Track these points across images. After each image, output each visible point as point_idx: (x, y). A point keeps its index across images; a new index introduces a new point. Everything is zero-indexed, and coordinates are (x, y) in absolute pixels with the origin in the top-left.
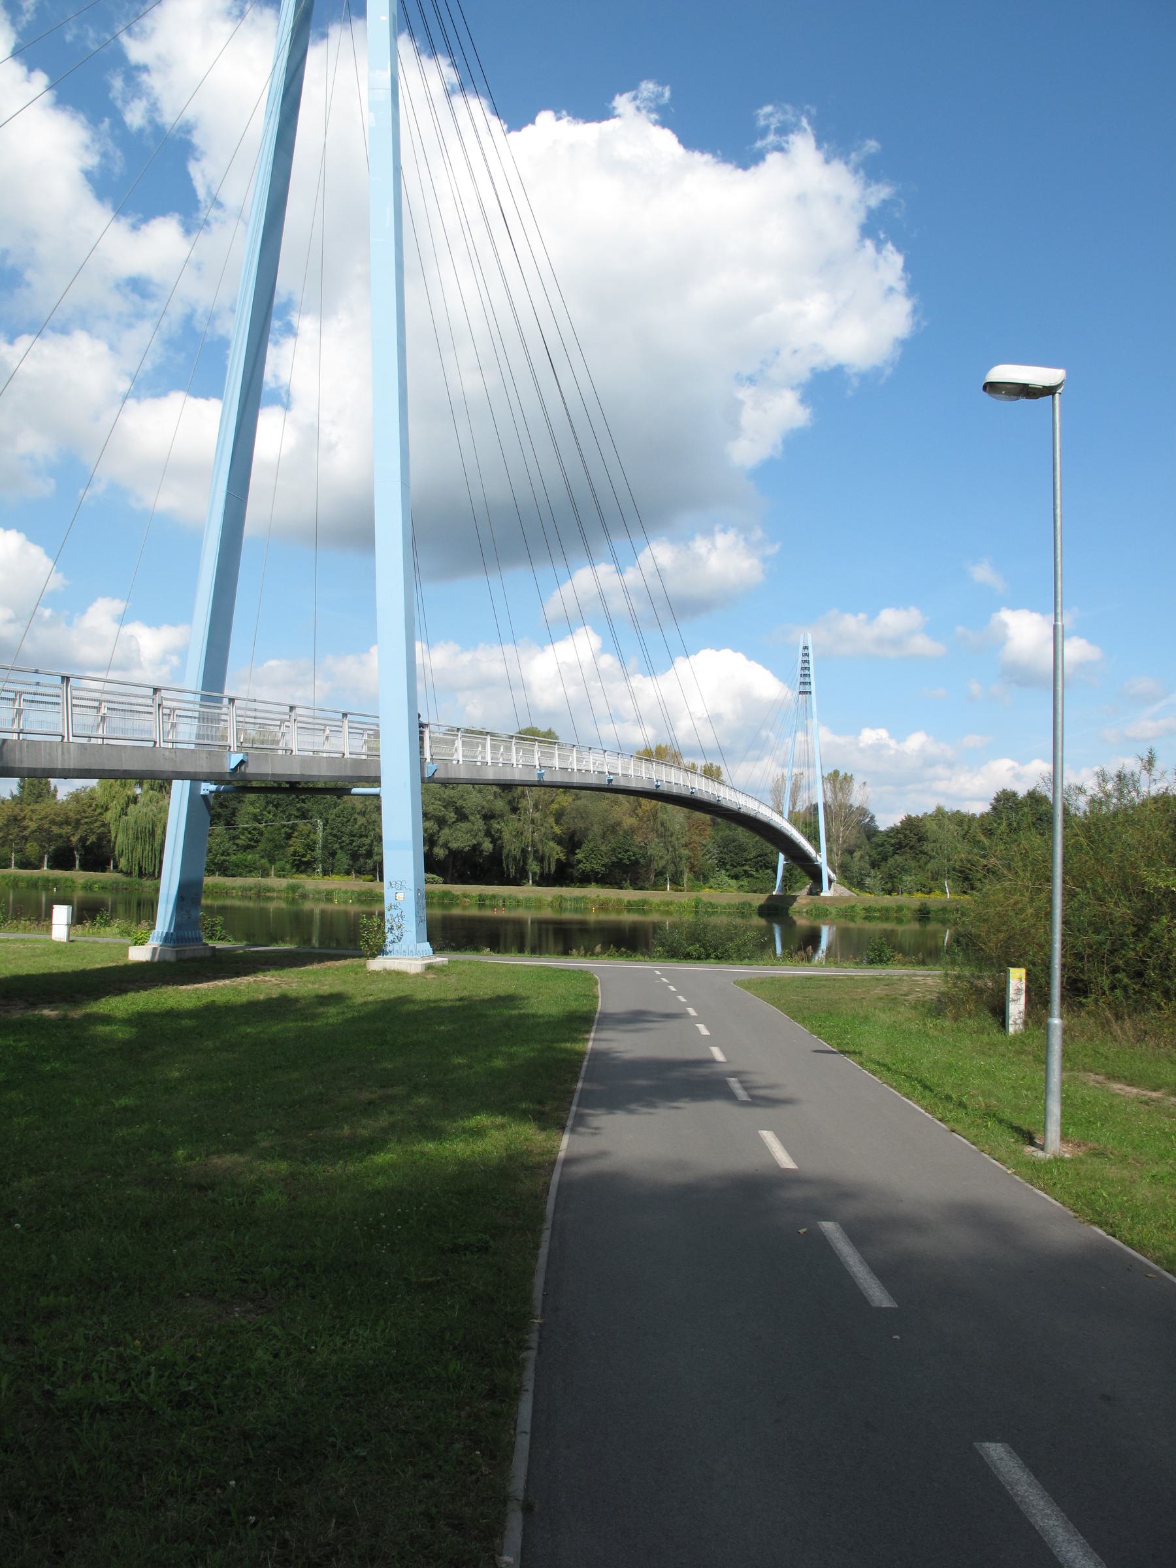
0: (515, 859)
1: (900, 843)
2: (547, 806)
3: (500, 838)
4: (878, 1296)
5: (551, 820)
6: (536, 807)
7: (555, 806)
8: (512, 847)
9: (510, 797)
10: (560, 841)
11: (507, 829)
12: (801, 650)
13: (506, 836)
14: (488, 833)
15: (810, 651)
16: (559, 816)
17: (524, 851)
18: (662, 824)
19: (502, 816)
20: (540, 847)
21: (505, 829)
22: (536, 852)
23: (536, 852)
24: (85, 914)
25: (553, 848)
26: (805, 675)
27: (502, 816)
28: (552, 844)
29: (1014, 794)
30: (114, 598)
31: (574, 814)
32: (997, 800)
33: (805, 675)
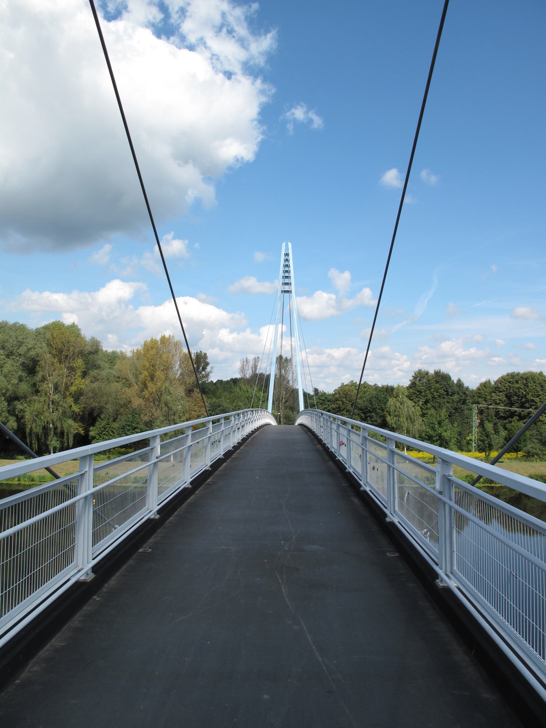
0: (37, 436)
1: (339, 408)
2: (67, 388)
3: (23, 417)
4: (474, 651)
5: (70, 400)
6: (56, 388)
7: (73, 389)
8: (33, 426)
9: (33, 382)
10: (75, 417)
11: (28, 410)
12: (283, 257)
13: (28, 416)
14: (12, 412)
15: (291, 257)
16: (77, 396)
17: (45, 429)
18: (166, 405)
19: (25, 397)
20: (59, 425)
21: (28, 410)
22: (56, 428)
23: (56, 428)
24: (475, 446)
25: (70, 426)
26: (287, 277)
27: (25, 397)
28: (70, 422)
29: (427, 373)
30: (60, 292)
31: (90, 394)
32: (415, 378)
33: (287, 277)
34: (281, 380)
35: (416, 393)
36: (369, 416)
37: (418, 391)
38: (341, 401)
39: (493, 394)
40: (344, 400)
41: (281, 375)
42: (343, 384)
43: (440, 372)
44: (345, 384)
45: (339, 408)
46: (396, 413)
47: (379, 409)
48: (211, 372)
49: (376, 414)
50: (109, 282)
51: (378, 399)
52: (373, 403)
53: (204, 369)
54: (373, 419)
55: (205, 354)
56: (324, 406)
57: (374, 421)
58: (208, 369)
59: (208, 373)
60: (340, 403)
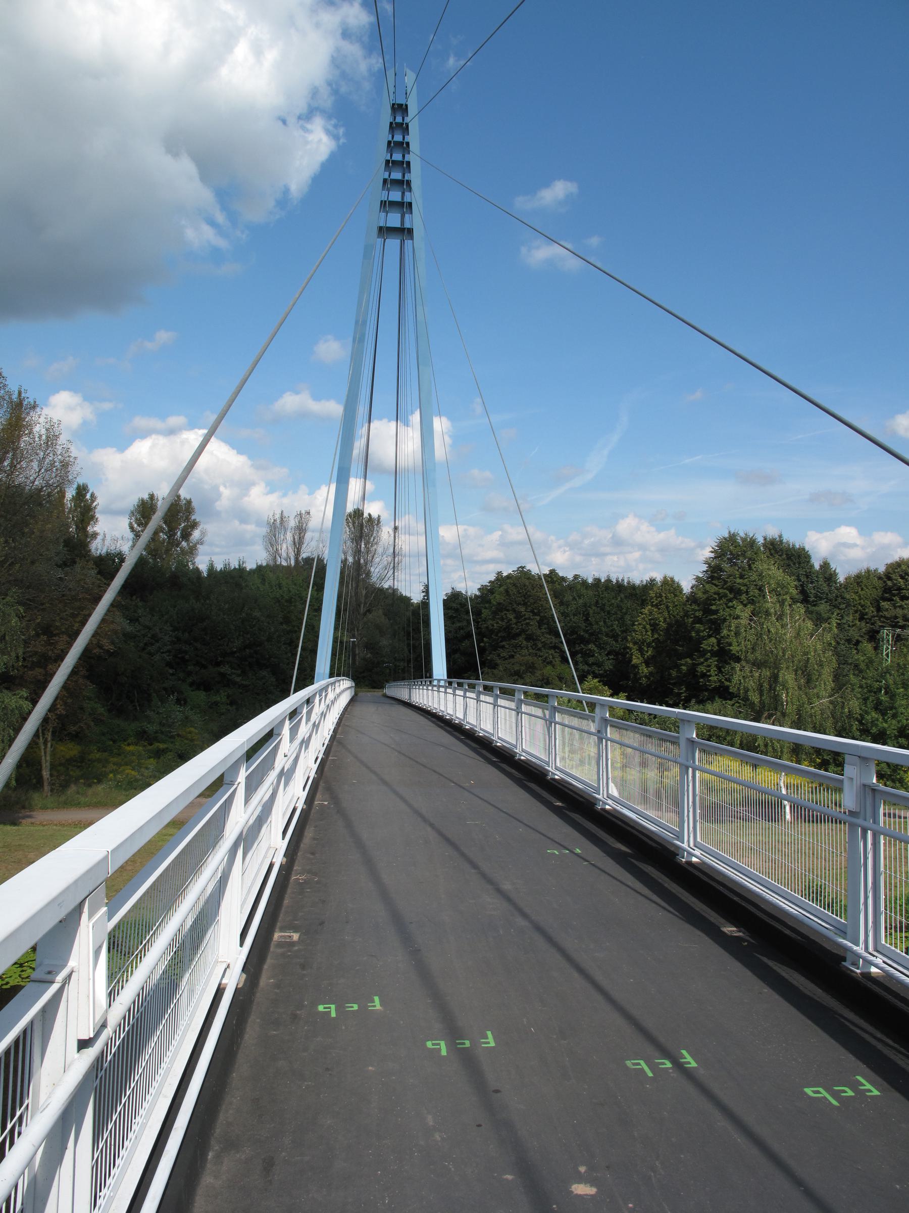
1: (508, 628)
15: (413, 120)
34: (355, 575)
35: (725, 596)
36: (581, 652)
37: (731, 590)
38: (514, 610)
39: (885, 604)
40: (522, 609)
41: (357, 563)
42: (499, 573)
43: (781, 541)
44: (505, 574)
45: (508, 628)
46: (758, 655)
47: (607, 635)
48: (200, 542)
49: (600, 647)
50: (54, 395)
51: (603, 609)
52: (592, 620)
53: (186, 536)
54: (591, 660)
55: (189, 502)
56: (458, 625)
57: (593, 664)
58: (196, 534)
59: (195, 546)
60: (511, 616)
